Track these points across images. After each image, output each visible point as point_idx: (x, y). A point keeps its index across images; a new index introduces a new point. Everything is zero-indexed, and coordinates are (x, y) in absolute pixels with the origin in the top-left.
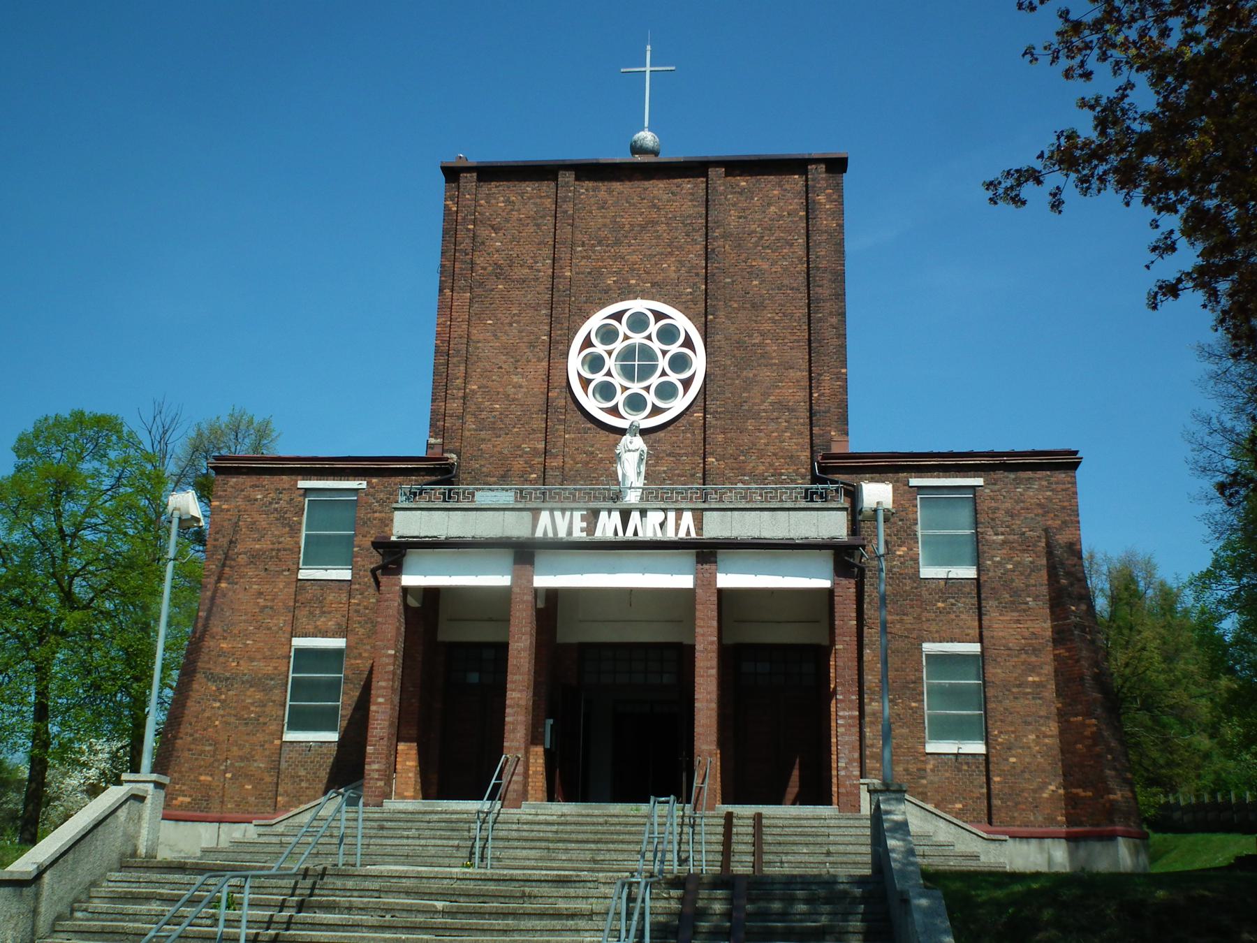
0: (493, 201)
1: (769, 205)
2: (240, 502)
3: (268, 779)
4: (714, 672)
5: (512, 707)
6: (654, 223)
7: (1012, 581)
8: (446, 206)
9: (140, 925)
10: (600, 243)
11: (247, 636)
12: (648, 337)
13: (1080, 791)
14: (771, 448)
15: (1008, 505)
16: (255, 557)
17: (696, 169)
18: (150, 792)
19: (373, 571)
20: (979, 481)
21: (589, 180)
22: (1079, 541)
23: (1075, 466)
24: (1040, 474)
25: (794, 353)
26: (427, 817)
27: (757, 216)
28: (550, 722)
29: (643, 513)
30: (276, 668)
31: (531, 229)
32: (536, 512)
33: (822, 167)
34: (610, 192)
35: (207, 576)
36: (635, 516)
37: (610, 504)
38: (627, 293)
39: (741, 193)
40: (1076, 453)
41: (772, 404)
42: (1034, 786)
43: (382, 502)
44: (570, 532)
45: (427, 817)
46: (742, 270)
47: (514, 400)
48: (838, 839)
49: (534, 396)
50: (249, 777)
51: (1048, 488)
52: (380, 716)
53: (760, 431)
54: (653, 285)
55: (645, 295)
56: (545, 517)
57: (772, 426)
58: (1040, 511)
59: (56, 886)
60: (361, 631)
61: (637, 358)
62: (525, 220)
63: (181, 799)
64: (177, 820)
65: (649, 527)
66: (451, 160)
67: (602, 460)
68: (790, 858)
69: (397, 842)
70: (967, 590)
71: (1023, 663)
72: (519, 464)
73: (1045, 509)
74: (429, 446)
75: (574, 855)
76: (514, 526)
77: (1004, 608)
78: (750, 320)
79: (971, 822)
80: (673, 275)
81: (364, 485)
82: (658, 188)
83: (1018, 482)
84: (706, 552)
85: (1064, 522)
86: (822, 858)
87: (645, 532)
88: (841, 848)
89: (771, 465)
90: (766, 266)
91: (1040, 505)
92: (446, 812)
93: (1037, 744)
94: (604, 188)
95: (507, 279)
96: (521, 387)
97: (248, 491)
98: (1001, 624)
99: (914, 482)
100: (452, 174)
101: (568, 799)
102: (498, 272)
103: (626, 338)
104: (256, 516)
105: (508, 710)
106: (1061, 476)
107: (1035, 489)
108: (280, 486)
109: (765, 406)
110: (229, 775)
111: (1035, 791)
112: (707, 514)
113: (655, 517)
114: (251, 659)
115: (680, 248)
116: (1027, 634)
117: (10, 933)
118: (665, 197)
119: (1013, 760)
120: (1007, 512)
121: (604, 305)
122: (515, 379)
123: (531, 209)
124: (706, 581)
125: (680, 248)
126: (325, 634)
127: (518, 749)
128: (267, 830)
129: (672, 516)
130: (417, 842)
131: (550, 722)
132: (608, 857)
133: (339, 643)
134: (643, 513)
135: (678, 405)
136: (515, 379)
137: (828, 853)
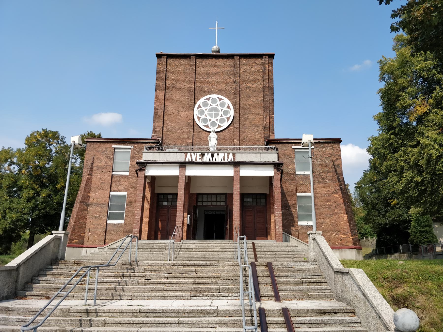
2: (94, 151)
4: (239, 200)
5: (179, 211)
8: (157, 66)
9: (57, 285)
13: (342, 236)
14: (252, 138)
15: (321, 154)
16: (98, 168)
17: (231, 56)
18: (63, 237)
19: (136, 171)
22: (341, 164)
23: (340, 142)
24: (330, 145)
25: (259, 110)
26: (153, 245)
28: (189, 216)
29: (218, 154)
30: (105, 201)
33: (267, 57)
34: (206, 63)
36: (216, 154)
37: (208, 152)
38: (210, 92)
39: (243, 64)
40: (340, 139)
41: (252, 125)
42: (329, 234)
43: (138, 152)
44: (196, 160)
49: (184, 122)
50: (96, 234)
51: (332, 149)
52: (138, 214)
54: (218, 90)
55: (215, 93)
56: (189, 154)
57: (253, 131)
59: (25, 271)
60: (131, 190)
61: (214, 111)
63: (75, 241)
64: (74, 247)
65: (217, 158)
66: (159, 52)
67: (203, 141)
73: (331, 155)
74: (153, 136)
75: (199, 256)
76: (180, 158)
81: (133, 147)
82: (220, 61)
83: (323, 147)
84: (236, 165)
86: (274, 256)
87: (218, 159)
89: (252, 142)
90: (251, 86)
91: (330, 154)
92: (158, 243)
93: (330, 222)
99: (294, 147)
100: (159, 56)
102: (173, 86)
103: (211, 105)
104: (100, 156)
105: (177, 212)
106: (336, 145)
108: (107, 147)
109: (251, 125)
110: (90, 233)
111: (329, 236)
113: (221, 155)
114: (97, 198)
116: (326, 190)
117: (6, 290)
118: (222, 65)
119: (323, 227)
120: (321, 156)
121: (204, 96)
122: (178, 117)
123: (182, 67)
124: (237, 173)
126: (120, 191)
127: (180, 224)
128: (102, 250)
129: (226, 154)
130: (150, 253)
131: (189, 216)
132: (209, 256)
133: (125, 193)
134: (218, 154)
135: (226, 125)
136: (178, 117)
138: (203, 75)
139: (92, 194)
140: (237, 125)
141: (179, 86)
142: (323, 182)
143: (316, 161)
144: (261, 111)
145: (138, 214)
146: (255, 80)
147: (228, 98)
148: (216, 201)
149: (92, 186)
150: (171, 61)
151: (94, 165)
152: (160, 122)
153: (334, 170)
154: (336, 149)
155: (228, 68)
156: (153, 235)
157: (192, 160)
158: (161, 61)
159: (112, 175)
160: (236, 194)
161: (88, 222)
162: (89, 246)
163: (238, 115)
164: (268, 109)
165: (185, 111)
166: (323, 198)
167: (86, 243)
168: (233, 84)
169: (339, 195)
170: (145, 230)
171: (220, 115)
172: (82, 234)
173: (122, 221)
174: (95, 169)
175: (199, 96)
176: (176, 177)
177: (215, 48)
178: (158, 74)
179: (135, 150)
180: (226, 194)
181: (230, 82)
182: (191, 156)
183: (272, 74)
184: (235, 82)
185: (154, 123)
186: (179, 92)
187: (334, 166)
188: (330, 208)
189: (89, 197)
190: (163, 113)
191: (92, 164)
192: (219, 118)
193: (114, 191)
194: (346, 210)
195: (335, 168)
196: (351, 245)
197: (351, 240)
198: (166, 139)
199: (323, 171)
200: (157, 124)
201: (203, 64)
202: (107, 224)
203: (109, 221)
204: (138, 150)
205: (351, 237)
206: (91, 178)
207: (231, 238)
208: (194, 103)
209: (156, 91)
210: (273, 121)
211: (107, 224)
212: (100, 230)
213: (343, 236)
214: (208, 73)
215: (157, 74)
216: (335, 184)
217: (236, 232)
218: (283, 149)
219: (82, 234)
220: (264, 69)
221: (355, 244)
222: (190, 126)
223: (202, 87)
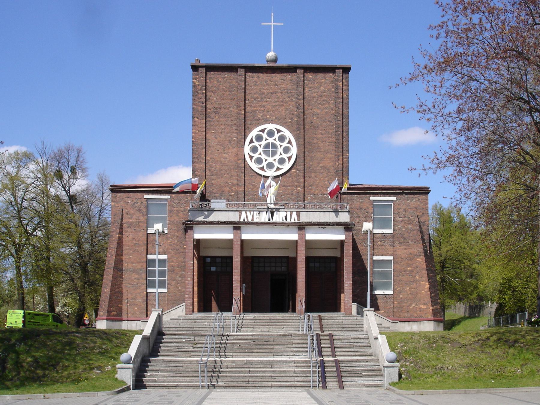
0: (212, 81)
1: (320, 86)
3: (143, 306)
6: (276, 92)
7: (404, 234)
8: (193, 82)
10: (255, 100)
11: (130, 254)
12: (274, 139)
14: (321, 185)
15: (404, 207)
16: (130, 225)
20: (394, 198)
21: (250, 73)
24: (416, 196)
26: (210, 318)
27: (316, 91)
31: (228, 93)
32: (240, 212)
34: (258, 77)
35: (113, 232)
39: (309, 80)
41: (321, 167)
43: (177, 204)
44: (253, 219)
45: (210, 318)
46: (311, 113)
47: (224, 164)
48: (346, 323)
50: (136, 305)
52: (189, 285)
53: (317, 177)
54: (276, 118)
55: (273, 122)
56: (244, 213)
57: (321, 176)
58: (415, 210)
60: (172, 252)
61: (271, 149)
62: (225, 88)
66: (194, 63)
68: (331, 329)
69: (203, 326)
70: (389, 237)
71: (406, 263)
72: (227, 189)
76: (233, 217)
77: (401, 244)
78: (313, 133)
79: (387, 317)
80: (284, 114)
82: (277, 77)
83: (408, 199)
84: (301, 227)
85: (423, 214)
88: (347, 326)
89: (321, 190)
90: (319, 112)
93: (410, 291)
94: (256, 76)
95: (220, 114)
96: (226, 158)
97: (125, 199)
98: (401, 251)
100: (195, 68)
101: (253, 311)
106: (423, 196)
107: (414, 201)
108: (137, 197)
111: (408, 306)
112: (301, 213)
114: (132, 263)
115: (286, 103)
116: (408, 253)
119: (401, 296)
121: (257, 126)
122: (224, 155)
124: (302, 237)
125: (286, 103)
129: (289, 213)
135: (287, 166)
136: (224, 155)
137: (343, 328)
138: (256, 96)
139: (125, 257)
140: (301, 167)
141: (224, 111)
142: (405, 242)
143: (397, 217)
144: (332, 149)
145: (189, 285)
146: (325, 104)
147: (288, 129)
148: (276, 267)
149: (124, 248)
150: (211, 75)
151: (124, 221)
152: (201, 162)
153: (418, 228)
154: (423, 201)
155: (289, 86)
156: (205, 307)
157: (248, 220)
158: (198, 75)
159: (147, 234)
160: (301, 261)
161: (124, 291)
162: (129, 318)
163: (302, 154)
164: (342, 146)
165: (233, 148)
166: (403, 263)
167: (124, 316)
168: (296, 109)
169: (422, 259)
170: (242, 310)
171: (279, 153)
172: (119, 305)
173: (165, 290)
174: (125, 226)
175: (250, 126)
176: (230, 241)
177: (271, 55)
178: (195, 94)
179: (173, 201)
180: (287, 258)
181: (292, 106)
182: (246, 214)
183: (348, 96)
184: (298, 107)
185: (193, 163)
186: (223, 120)
187: (419, 223)
188: (410, 274)
189: (122, 261)
190: (204, 151)
191: (122, 219)
192: (277, 157)
193: (152, 254)
194: (428, 277)
195: (420, 226)
196: (430, 316)
197: (431, 311)
198: (210, 186)
199: (406, 229)
200: (197, 165)
201: (255, 79)
202: (147, 293)
203: (149, 290)
204: (177, 201)
205: (431, 308)
206: (122, 237)
207: (294, 310)
208: (245, 136)
209: (193, 118)
210: (348, 161)
211: (147, 293)
212: (140, 300)
213: (423, 307)
214: (262, 93)
215: (194, 93)
216: (419, 245)
217: (301, 305)
218: (358, 200)
219: (119, 305)
220: (337, 88)
221: (434, 315)
222: (241, 167)
223: (254, 113)
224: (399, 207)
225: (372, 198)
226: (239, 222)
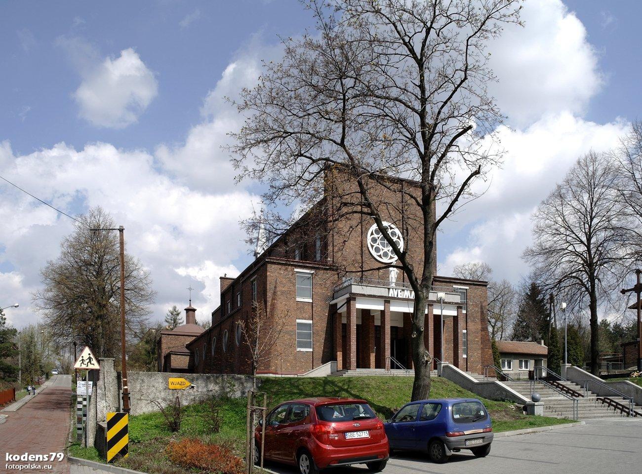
20: (467, 288)
83: (476, 289)
106: (484, 288)
107: (479, 290)
151: (278, 289)
224: (470, 294)
225: (454, 286)
226: (389, 297)
